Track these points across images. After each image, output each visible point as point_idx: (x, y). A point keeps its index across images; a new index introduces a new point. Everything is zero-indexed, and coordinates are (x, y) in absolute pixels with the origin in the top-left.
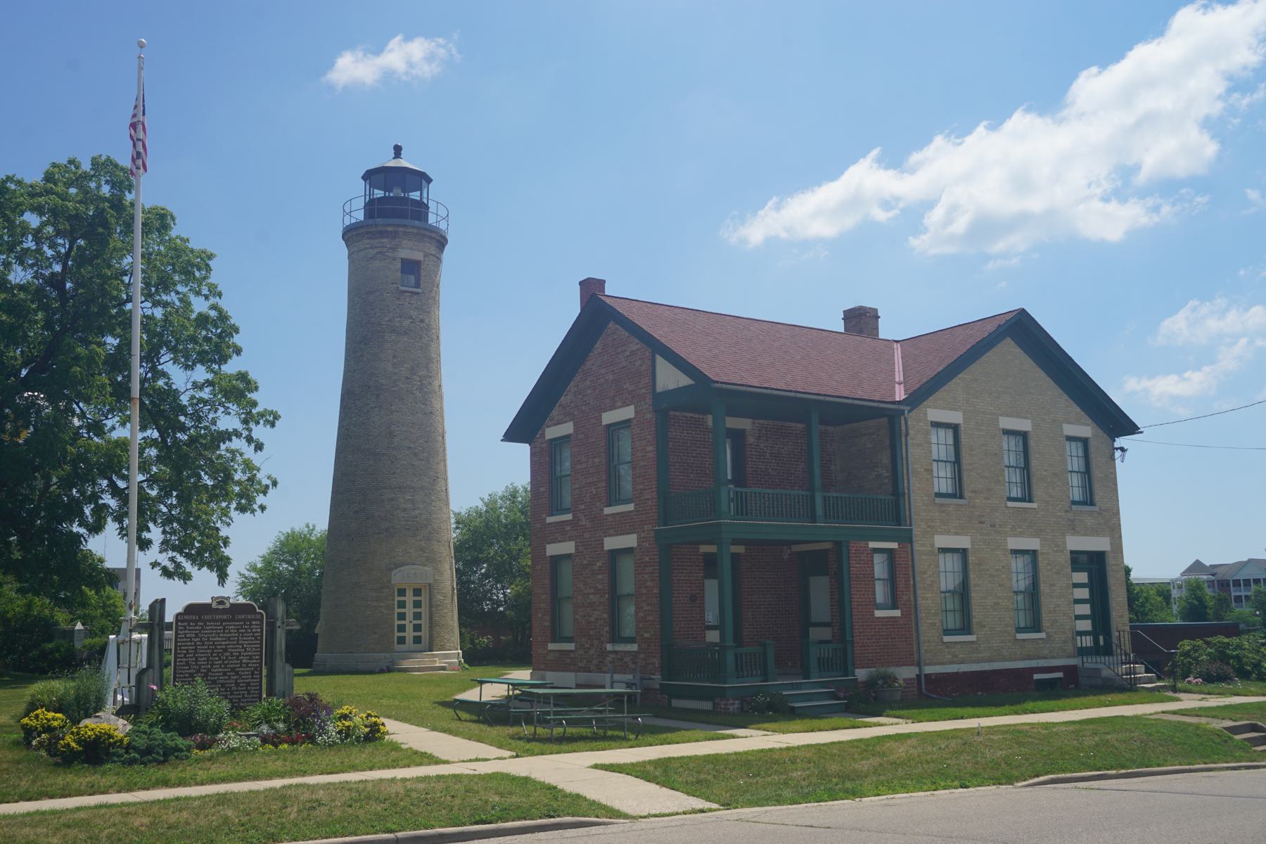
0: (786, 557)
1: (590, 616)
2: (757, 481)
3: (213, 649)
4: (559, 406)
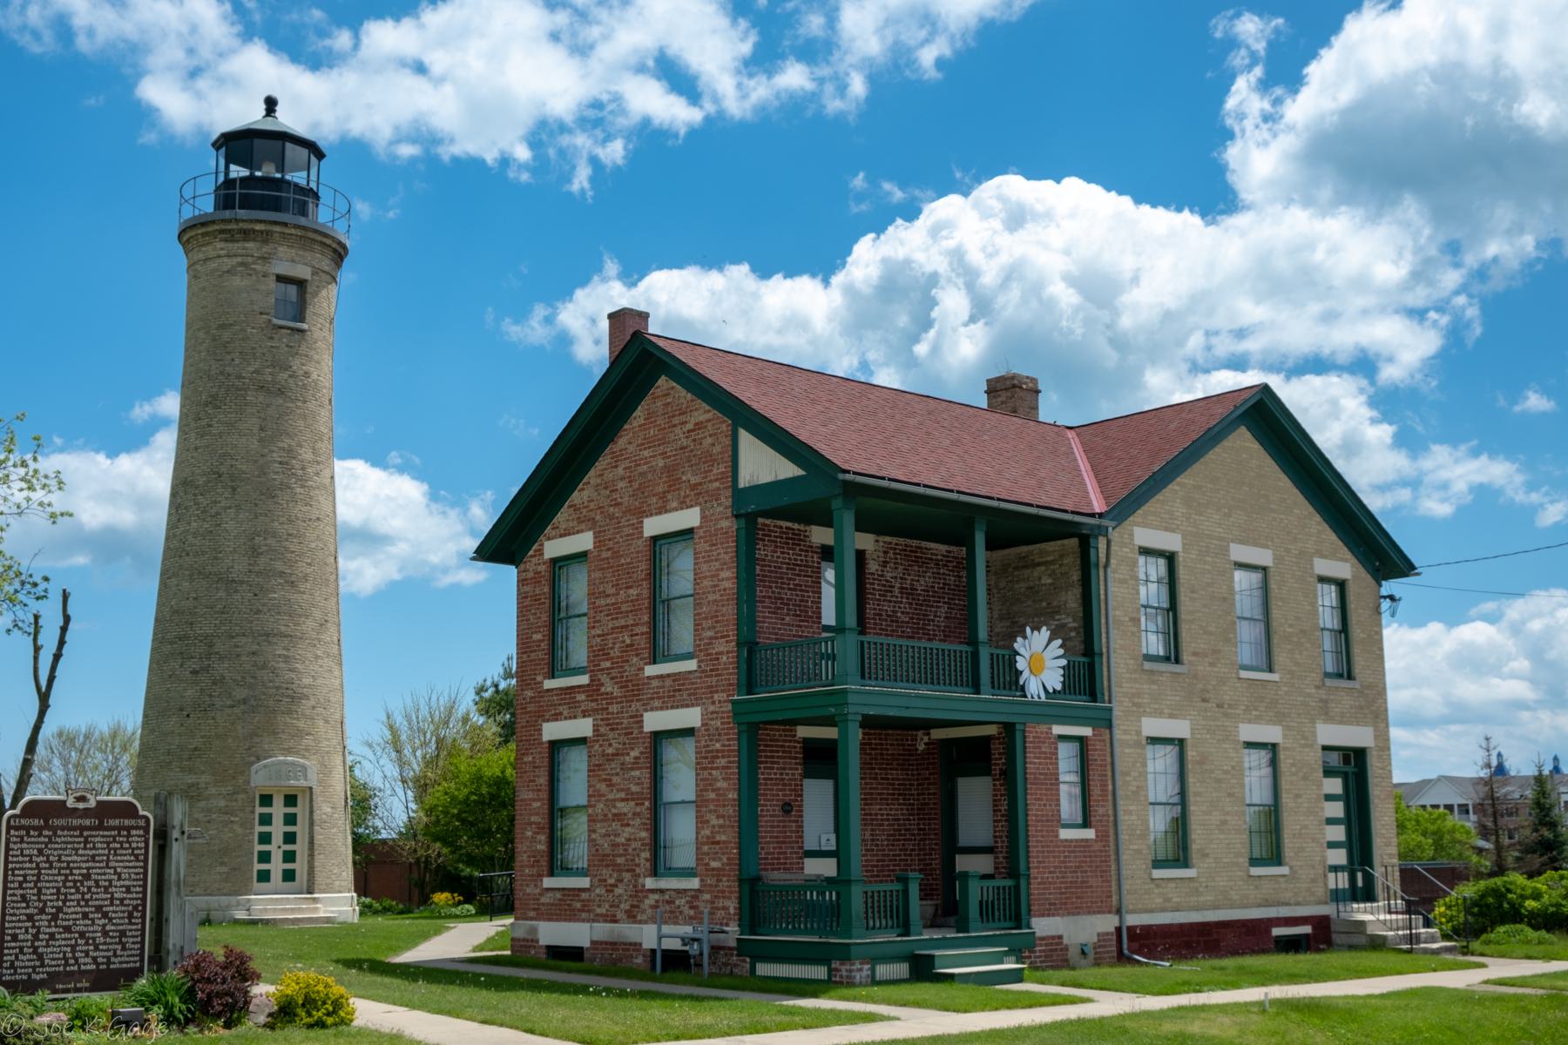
0: (921, 747)
1: (617, 835)
2: (881, 629)
3: (66, 875)
4: (570, 507)
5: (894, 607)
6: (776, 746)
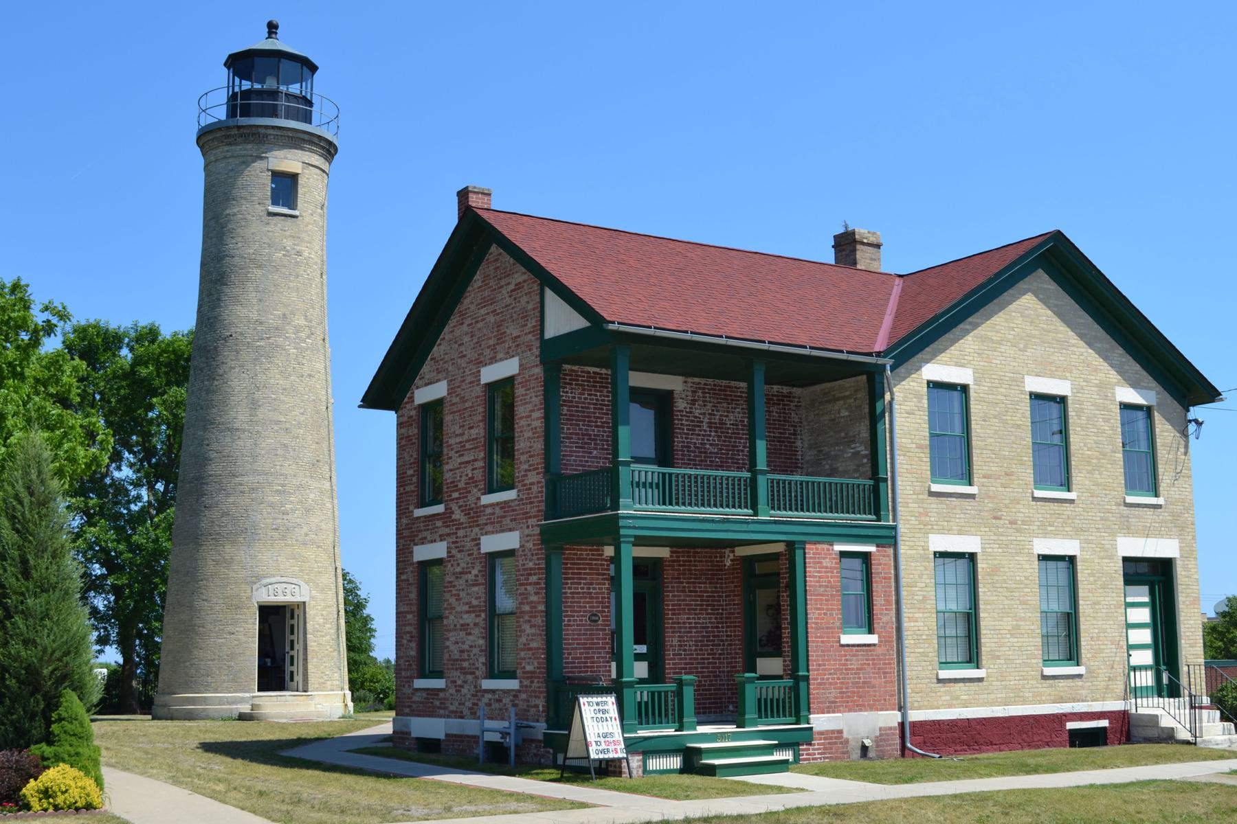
0: (728, 563)
1: (463, 643)
4: (432, 359)
5: (702, 440)
6: (583, 564)
